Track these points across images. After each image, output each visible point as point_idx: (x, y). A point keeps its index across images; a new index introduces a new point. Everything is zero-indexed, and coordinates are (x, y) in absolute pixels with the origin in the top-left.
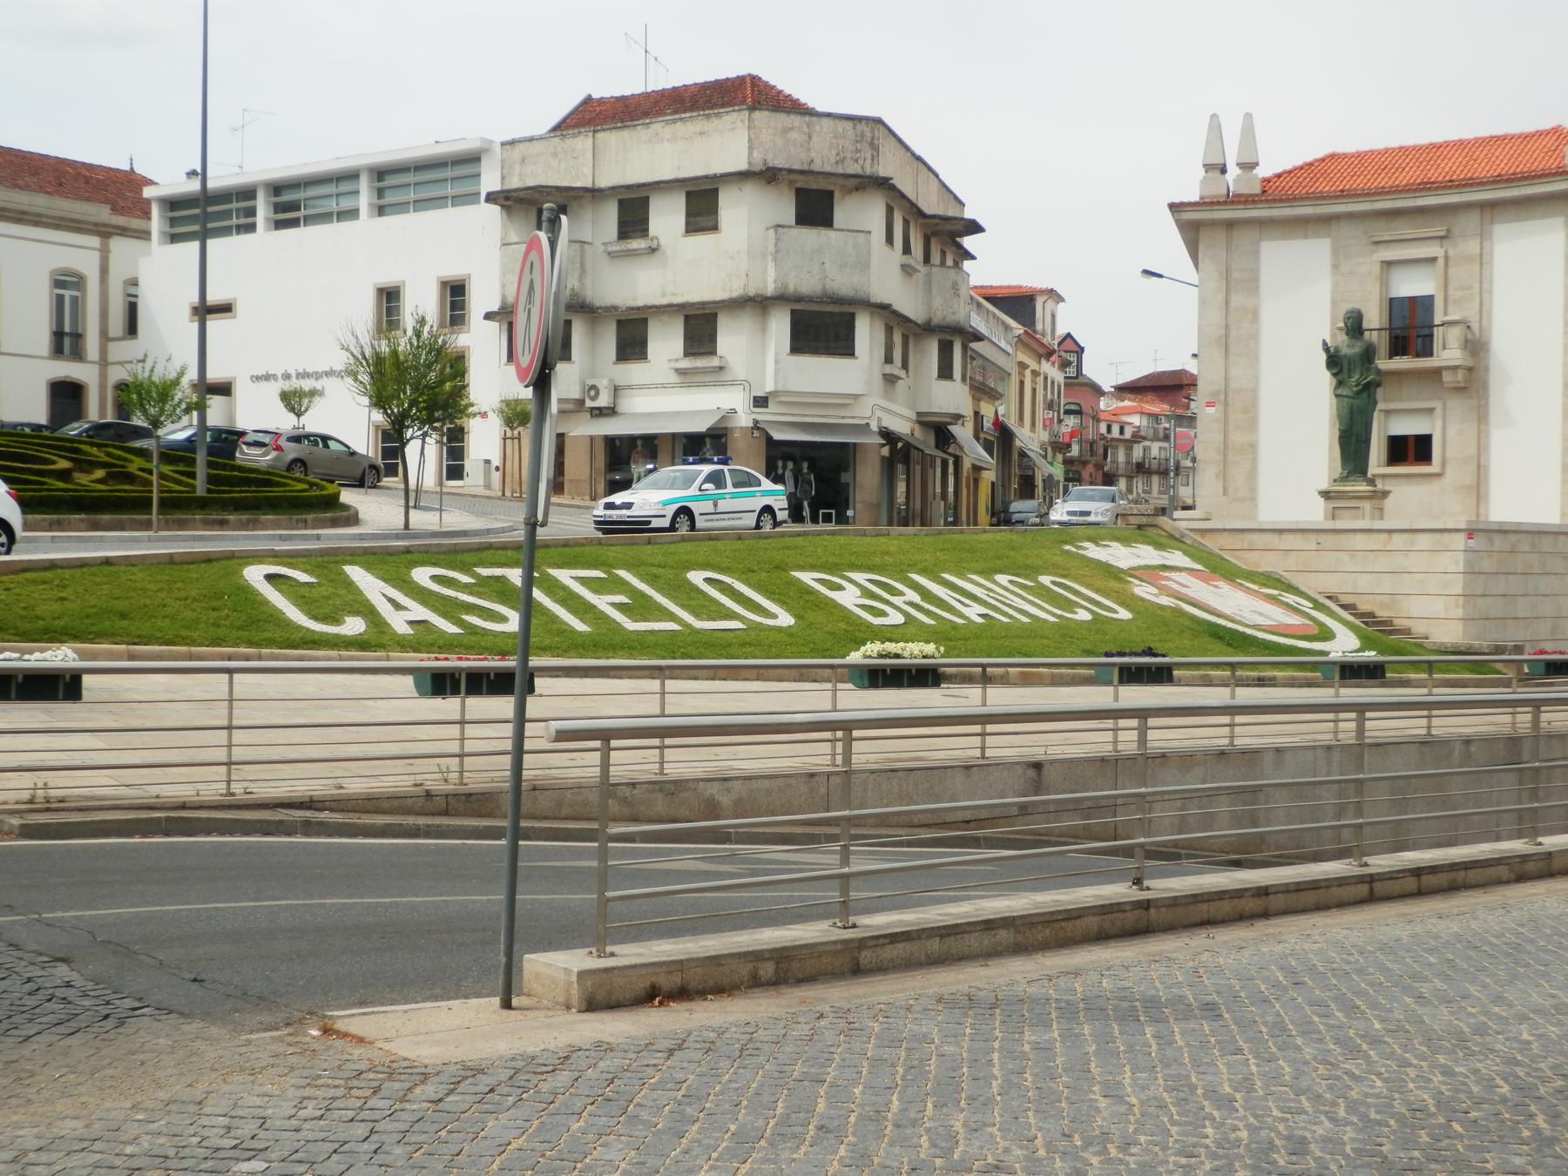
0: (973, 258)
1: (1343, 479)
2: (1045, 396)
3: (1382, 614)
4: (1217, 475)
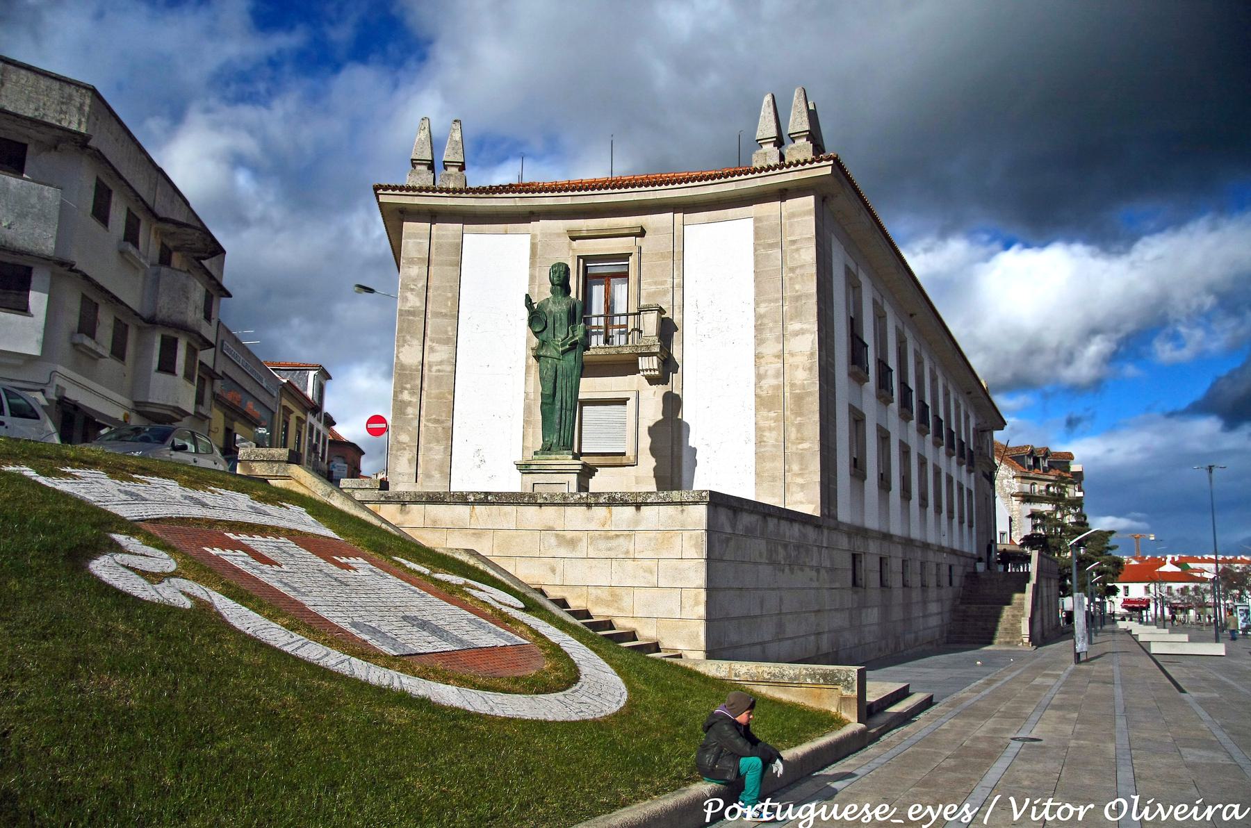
0: (229, 295)
1: (547, 449)
2: (311, 441)
3: (599, 613)
4: (410, 461)
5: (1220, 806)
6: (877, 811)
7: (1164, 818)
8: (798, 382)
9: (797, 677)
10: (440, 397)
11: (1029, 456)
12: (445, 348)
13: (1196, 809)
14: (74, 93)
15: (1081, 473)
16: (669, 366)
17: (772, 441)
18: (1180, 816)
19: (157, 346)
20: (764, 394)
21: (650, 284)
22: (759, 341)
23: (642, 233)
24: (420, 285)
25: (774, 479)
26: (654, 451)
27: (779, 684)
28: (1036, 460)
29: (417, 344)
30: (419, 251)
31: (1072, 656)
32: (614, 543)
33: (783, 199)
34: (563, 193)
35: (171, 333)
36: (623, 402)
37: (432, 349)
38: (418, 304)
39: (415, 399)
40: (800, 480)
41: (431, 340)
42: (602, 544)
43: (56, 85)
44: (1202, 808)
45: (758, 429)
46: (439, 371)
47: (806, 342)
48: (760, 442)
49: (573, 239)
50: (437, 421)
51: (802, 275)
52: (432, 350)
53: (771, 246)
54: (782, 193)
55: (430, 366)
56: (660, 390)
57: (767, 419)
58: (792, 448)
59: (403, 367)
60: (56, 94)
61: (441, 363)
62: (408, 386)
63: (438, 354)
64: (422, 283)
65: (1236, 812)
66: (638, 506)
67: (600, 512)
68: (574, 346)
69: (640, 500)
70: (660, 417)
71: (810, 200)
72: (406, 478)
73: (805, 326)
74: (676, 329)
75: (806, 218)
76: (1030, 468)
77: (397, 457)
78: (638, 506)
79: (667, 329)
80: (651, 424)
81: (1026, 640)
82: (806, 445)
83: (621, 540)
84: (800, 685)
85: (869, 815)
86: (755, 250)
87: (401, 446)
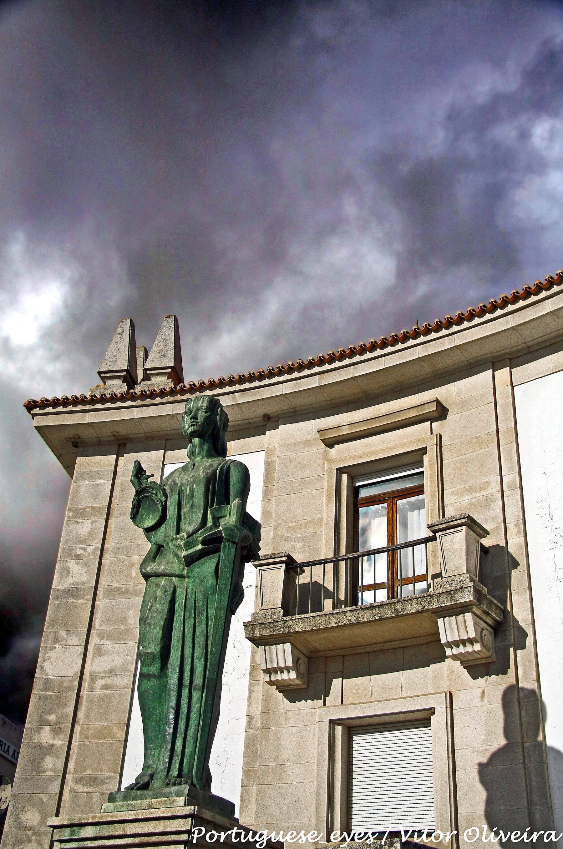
5: (542, 832)
6: (309, 836)
7: (504, 840)
13: (525, 835)
16: (503, 639)
18: (515, 839)
21: (460, 494)
24: (90, 548)
29: (75, 644)
30: (95, 498)
36: (422, 719)
37: (99, 652)
38: (84, 578)
39: (60, 742)
44: (530, 834)
46: (106, 687)
49: (330, 444)
52: (99, 652)
56: (495, 685)
61: (111, 672)
62: (52, 718)
65: (553, 836)
74: (515, 564)
79: (495, 569)
80: (484, 759)
85: (304, 838)
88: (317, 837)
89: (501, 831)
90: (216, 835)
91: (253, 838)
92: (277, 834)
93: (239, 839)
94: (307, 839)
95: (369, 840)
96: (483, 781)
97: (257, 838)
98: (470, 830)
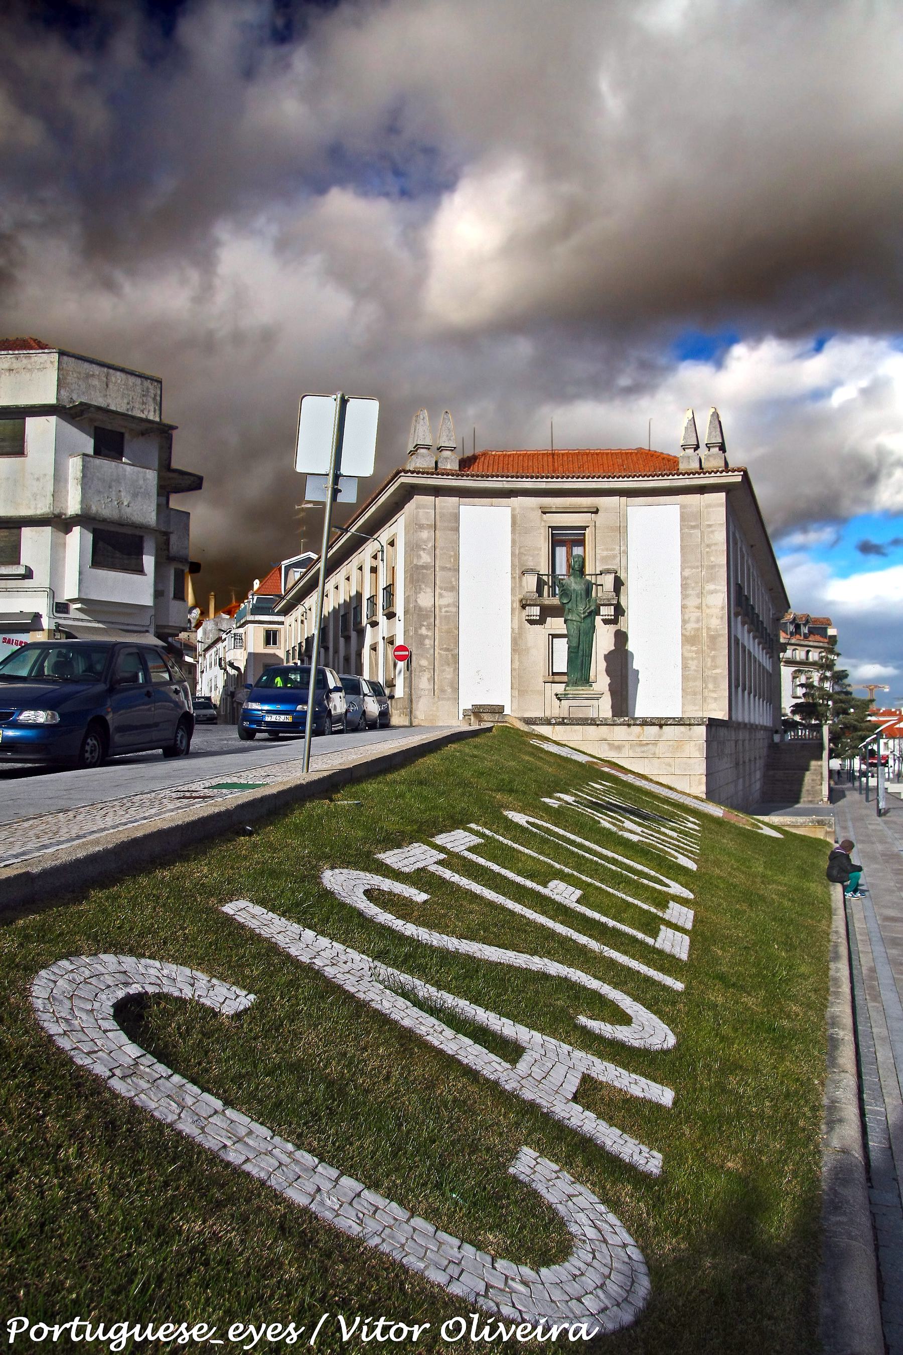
4: (429, 680)
6: (195, 1331)
7: (505, 1338)
8: (712, 627)
9: (804, 823)
10: (449, 632)
11: (791, 623)
12: (450, 594)
14: (150, 386)
15: (835, 636)
17: (693, 668)
19: (172, 578)
20: (688, 634)
21: (603, 550)
22: (684, 596)
23: (596, 512)
25: (695, 694)
26: (608, 672)
27: (794, 826)
28: (798, 627)
29: (429, 590)
30: (427, 519)
31: (875, 813)
32: (645, 748)
33: (702, 493)
34: (539, 480)
35: (181, 566)
37: (441, 595)
38: (429, 560)
39: (430, 634)
40: (715, 695)
41: (441, 588)
42: (638, 749)
43: (139, 381)
45: (684, 658)
46: (447, 612)
47: (718, 598)
48: (685, 667)
50: (447, 650)
51: (716, 551)
52: (441, 595)
53: (693, 527)
54: (702, 490)
55: (440, 608)
56: (612, 628)
57: (691, 651)
58: (708, 673)
59: (420, 609)
60: (139, 389)
61: (448, 606)
62: (425, 623)
63: (447, 599)
64: (431, 544)
65: (583, 1332)
66: (661, 726)
67: (637, 729)
68: (590, 613)
69: (663, 722)
70: (613, 648)
71: (723, 495)
72: (427, 692)
73: (718, 588)
74: (623, 584)
75: (720, 509)
76: (792, 634)
77: (419, 677)
78: (661, 726)
79: (619, 584)
81: (826, 799)
82: (718, 671)
83: (650, 746)
84: (805, 827)
85: (186, 1335)
86: (681, 529)
87: (422, 669)
88: (207, 1333)
89: (500, 1324)
90: (46, 1329)
91: (104, 1334)
92: (143, 1329)
93: (82, 1336)
94: (191, 1336)
95: (290, 1338)
96: (605, 660)
97: (111, 1334)
98: (451, 1322)
